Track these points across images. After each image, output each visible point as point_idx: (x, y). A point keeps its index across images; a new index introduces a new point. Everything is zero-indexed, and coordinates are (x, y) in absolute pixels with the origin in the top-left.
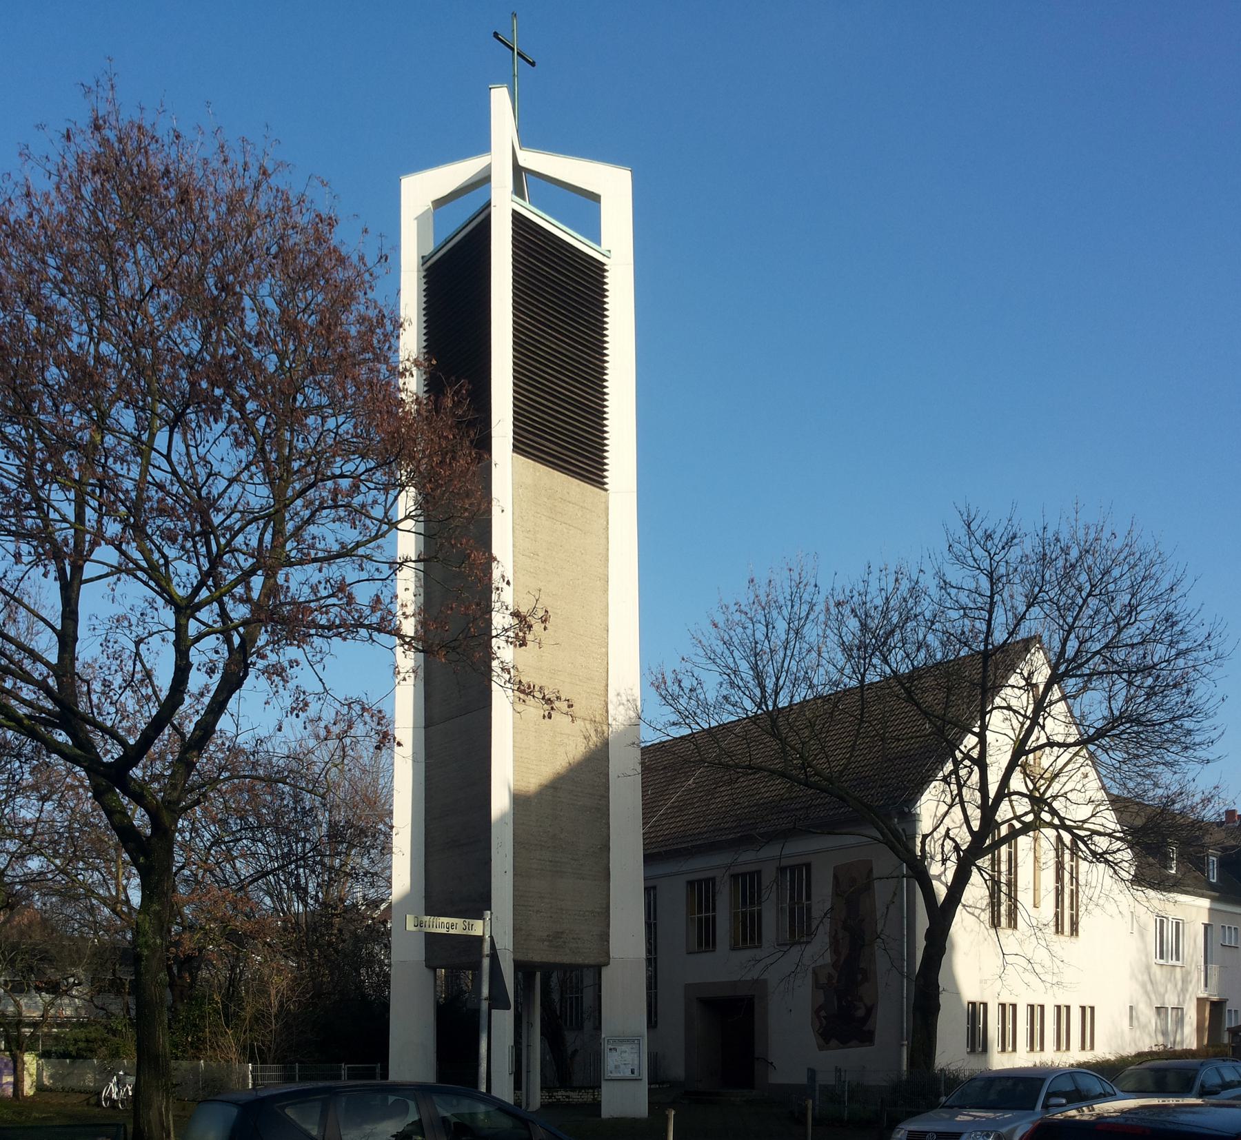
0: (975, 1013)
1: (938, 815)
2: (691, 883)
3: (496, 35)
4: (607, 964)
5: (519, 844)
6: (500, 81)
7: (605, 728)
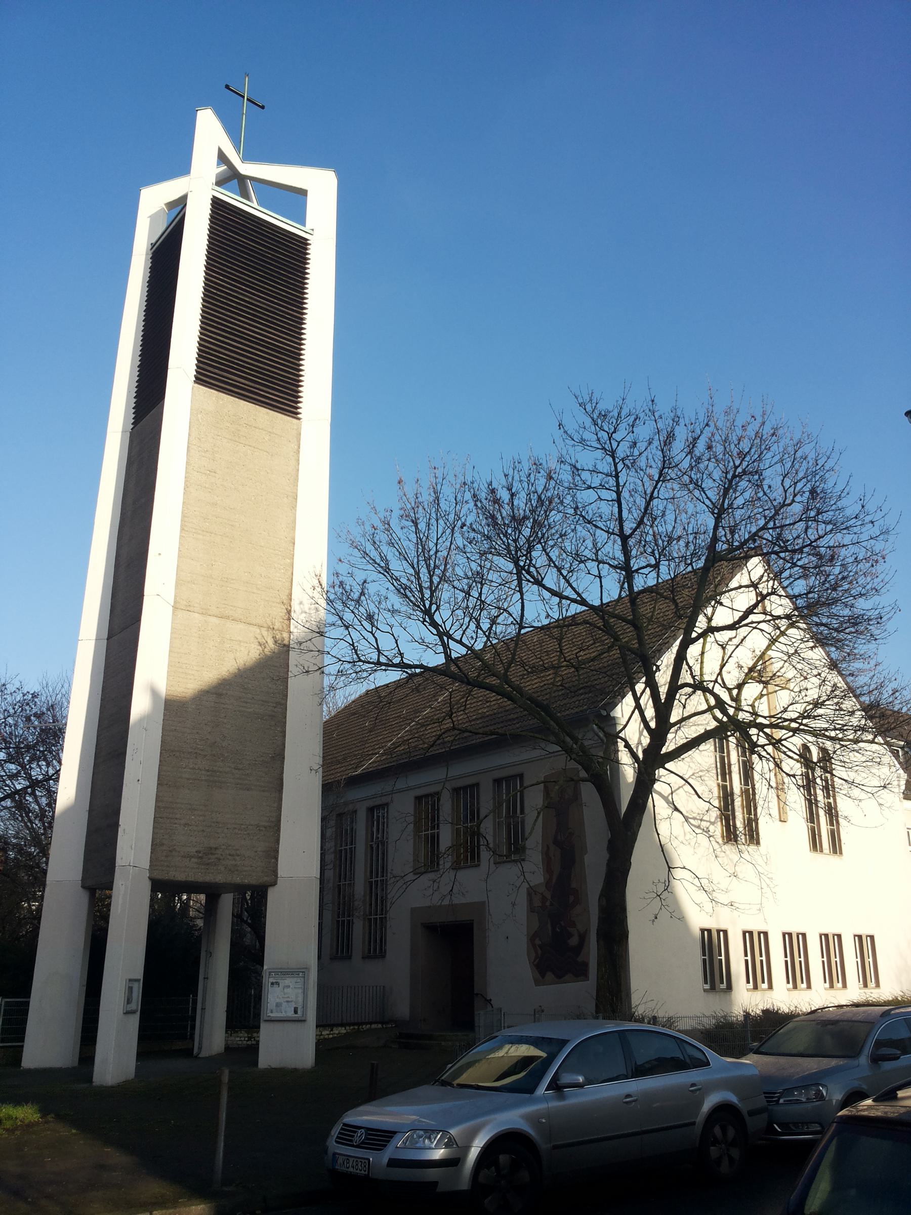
0: (711, 945)
1: (630, 718)
2: (418, 799)
3: (227, 87)
4: (274, 884)
5: (170, 751)
6: (205, 104)
7: (285, 635)
